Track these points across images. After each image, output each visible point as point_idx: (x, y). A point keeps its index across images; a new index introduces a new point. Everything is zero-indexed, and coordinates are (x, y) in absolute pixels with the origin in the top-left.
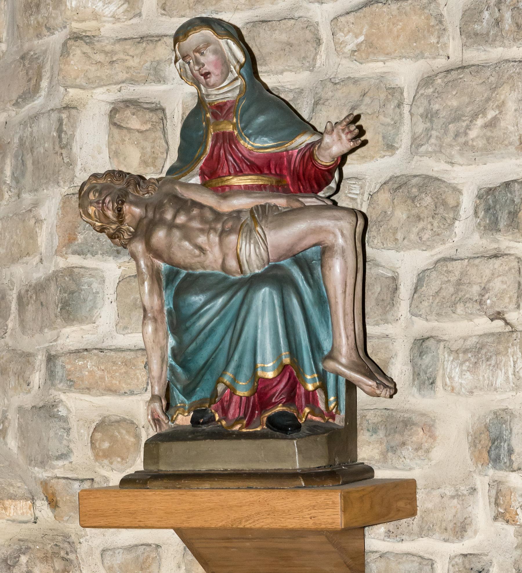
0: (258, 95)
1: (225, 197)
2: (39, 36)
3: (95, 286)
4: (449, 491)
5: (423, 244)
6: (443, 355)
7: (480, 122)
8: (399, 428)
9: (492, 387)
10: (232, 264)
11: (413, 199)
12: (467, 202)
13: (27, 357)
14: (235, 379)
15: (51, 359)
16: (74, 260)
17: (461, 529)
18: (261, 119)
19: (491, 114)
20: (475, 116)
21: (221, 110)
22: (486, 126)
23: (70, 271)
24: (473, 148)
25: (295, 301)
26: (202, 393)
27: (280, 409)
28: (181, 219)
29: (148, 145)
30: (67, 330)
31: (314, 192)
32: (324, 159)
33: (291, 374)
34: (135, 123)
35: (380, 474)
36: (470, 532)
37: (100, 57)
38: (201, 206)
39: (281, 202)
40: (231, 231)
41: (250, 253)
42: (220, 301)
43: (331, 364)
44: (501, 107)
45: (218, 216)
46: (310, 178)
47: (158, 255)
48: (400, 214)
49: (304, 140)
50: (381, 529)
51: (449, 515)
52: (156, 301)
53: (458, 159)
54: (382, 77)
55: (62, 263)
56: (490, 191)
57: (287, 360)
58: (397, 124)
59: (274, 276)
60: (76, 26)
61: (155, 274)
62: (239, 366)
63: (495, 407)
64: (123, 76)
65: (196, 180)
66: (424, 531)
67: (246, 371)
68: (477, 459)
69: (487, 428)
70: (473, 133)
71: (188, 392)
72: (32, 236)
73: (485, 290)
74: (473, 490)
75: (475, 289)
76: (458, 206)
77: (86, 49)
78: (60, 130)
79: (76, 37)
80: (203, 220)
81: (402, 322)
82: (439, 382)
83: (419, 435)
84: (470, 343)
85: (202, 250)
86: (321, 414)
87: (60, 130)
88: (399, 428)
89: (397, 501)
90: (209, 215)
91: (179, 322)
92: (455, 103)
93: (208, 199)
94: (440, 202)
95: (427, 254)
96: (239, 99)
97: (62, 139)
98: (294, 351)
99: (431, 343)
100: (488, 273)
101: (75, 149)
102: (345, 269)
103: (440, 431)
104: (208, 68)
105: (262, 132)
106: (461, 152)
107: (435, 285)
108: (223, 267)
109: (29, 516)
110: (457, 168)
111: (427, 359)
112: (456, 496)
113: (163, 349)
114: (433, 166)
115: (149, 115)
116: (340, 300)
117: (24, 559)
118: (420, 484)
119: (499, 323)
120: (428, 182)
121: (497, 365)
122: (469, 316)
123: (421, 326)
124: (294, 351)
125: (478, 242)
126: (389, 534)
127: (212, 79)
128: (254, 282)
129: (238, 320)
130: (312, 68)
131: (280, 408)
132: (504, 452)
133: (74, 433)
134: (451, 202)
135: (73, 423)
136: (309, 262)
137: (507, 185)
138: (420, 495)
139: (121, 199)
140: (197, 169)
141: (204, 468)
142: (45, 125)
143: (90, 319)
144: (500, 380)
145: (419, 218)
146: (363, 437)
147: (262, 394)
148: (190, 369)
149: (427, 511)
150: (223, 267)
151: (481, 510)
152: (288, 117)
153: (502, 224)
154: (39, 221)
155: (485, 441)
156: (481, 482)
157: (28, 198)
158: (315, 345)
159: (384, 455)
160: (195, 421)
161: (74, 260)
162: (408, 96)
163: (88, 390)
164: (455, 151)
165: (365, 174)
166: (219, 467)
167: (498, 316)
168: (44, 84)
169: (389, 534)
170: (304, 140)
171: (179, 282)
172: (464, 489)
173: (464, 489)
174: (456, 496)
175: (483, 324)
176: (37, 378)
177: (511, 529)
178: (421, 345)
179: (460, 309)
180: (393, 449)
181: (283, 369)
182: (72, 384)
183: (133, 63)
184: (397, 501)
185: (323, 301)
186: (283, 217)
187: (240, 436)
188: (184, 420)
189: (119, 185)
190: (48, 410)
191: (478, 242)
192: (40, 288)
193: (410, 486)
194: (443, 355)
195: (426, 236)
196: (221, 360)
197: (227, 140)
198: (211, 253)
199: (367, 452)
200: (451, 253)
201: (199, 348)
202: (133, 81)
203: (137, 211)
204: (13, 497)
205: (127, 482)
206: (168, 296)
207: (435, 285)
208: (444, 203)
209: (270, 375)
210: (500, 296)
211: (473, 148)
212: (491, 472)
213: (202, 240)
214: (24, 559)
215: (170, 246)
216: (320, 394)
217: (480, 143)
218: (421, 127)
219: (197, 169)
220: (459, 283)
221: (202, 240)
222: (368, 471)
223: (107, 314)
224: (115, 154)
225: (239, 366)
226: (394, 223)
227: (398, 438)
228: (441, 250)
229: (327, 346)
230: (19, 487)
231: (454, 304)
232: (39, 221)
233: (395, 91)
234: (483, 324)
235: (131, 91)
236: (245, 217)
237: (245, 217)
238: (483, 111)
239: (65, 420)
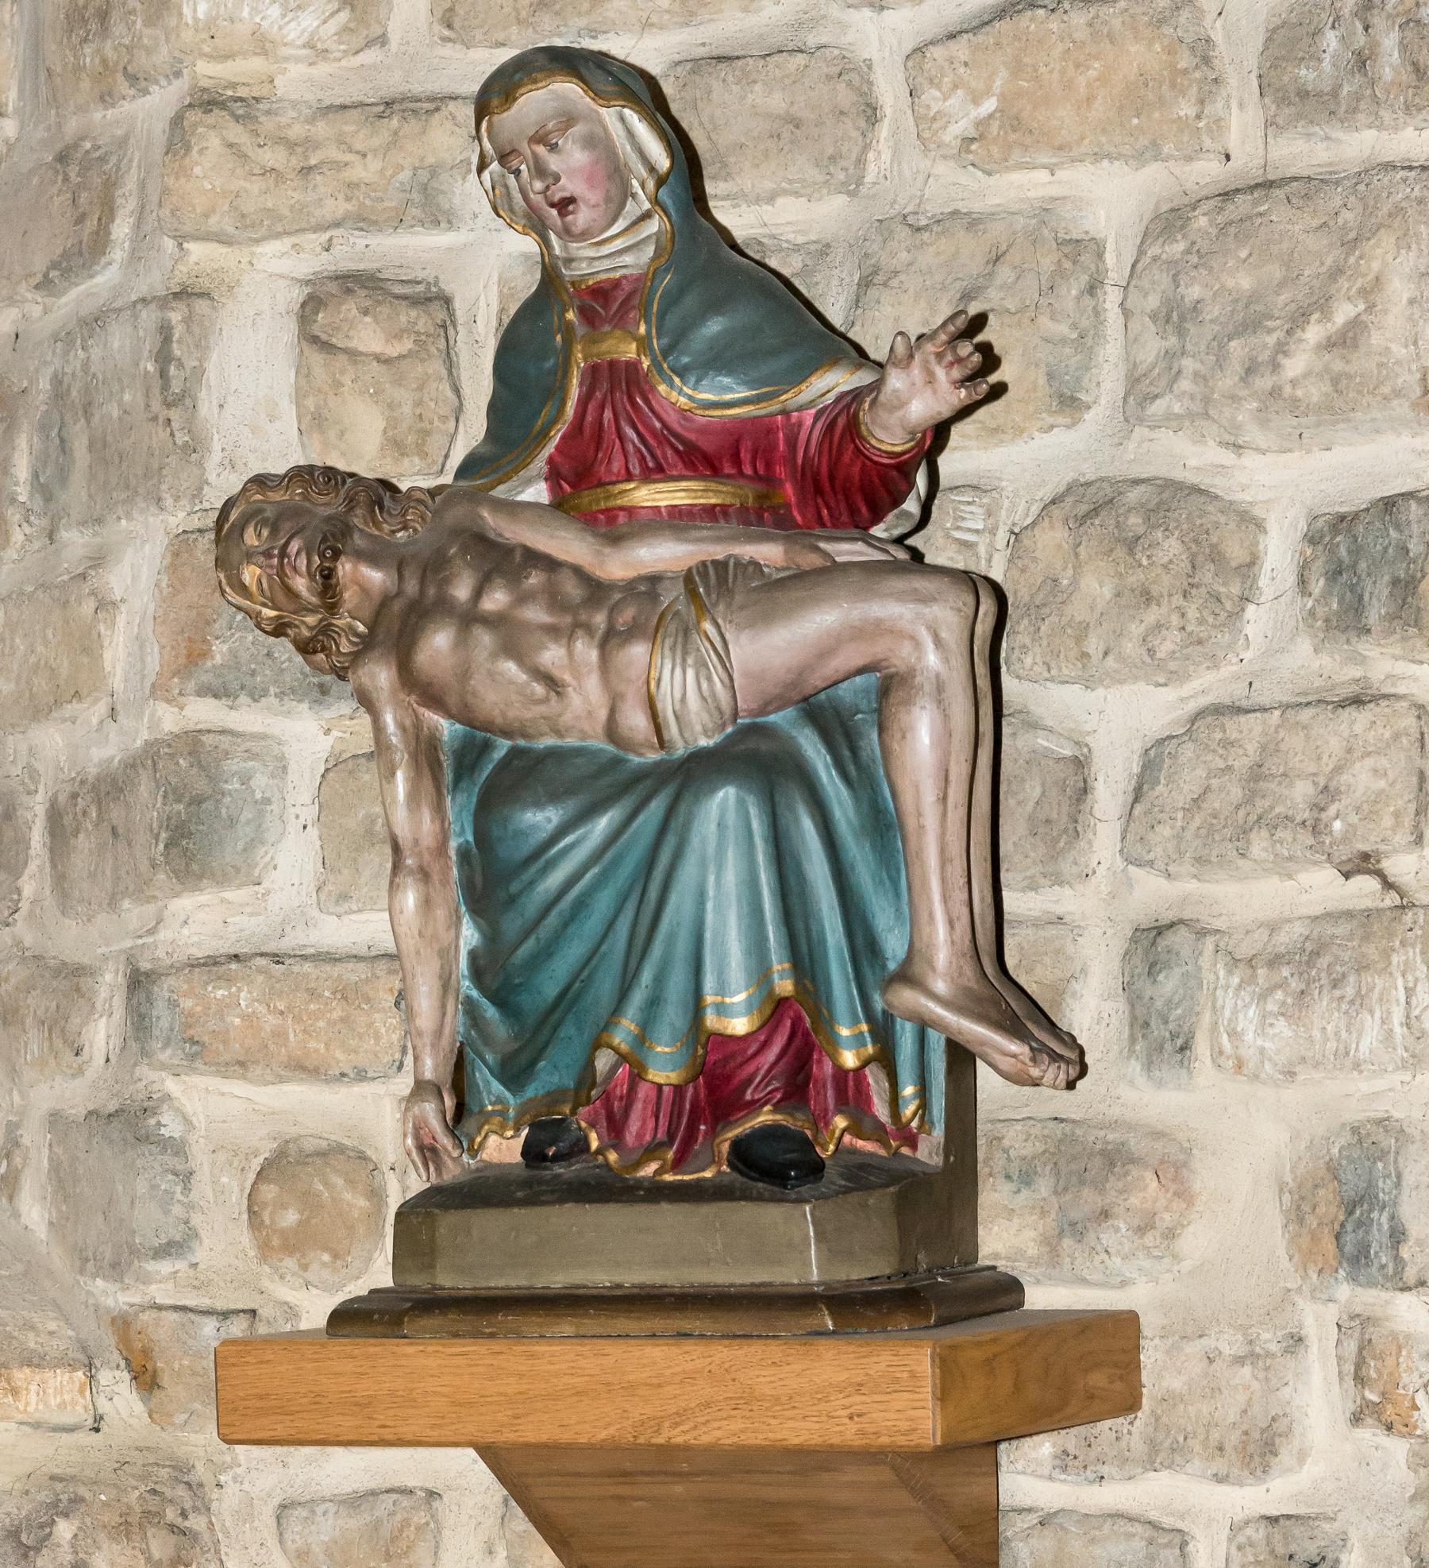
0: (707, 261)
1: (615, 539)
2: (107, 98)
3: (261, 782)
4: (1229, 1344)
5: (1158, 669)
6: (1214, 971)
7: (1313, 333)
8: (1093, 1170)
9: (1347, 1060)
10: (636, 721)
11: (1132, 545)
12: (1279, 553)
13: (74, 978)
14: (642, 1038)
15: (139, 982)
16: (204, 712)
17: (1261, 1447)
18: (714, 326)
19: (1344, 312)
20: (1299, 318)
21: (604, 302)
22: (1330, 345)
23: (192, 742)
24: (1295, 406)
25: (808, 824)
26: (552, 1075)
27: (766, 1120)
28: (496, 600)
29: (405, 398)
30: (185, 903)
31: (859, 524)
32: (888, 435)
33: (796, 1023)
34: (369, 337)
35: (1039, 1297)
36: (1285, 1456)
37: (273, 157)
38: (551, 564)
39: (769, 553)
40: (632, 633)
41: (685, 693)
42: (603, 824)
43: (907, 997)
44: (1371, 292)
45: (596, 590)
46: (849, 488)
47: (433, 698)
48: (1096, 586)
49: (833, 382)
50: (1044, 1447)
51: (1229, 1408)
52: (428, 823)
53: (1253, 434)
54: (1045, 211)
55: (169, 720)
56: (1342, 522)
57: (785, 986)
58: (1086, 340)
59: (750, 756)
60: (208, 71)
61: (425, 751)
62: (654, 1002)
63: (1355, 1113)
64: (337, 207)
65: (537, 492)
66: (1162, 1454)
67: (673, 1016)
68: (1305, 1255)
69: (1334, 1171)
70: (1295, 365)
71: (514, 1073)
72: (88, 646)
73: (1328, 793)
74: (1296, 1341)
75: (1302, 792)
76: (1253, 563)
77: (237, 133)
78: (164, 357)
79: (209, 101)
80: (556, 601)
81: (1101, 881)
82: (1202, 1046)
83: (1148, 1191)
84: (1287, 938)
85: (552, 683)
86: (878, 1133)
87: (164, 357)
88: (1093, 1170)
89: (1088, 1372)
90: (572, 589)
91: (489, 880)
92: (1245, 282)
93: (569, 545)
94: (1205, 553)
95: (1169, 694)
96: (655, 272)
97: (171, 380)
98: (805, 959)
99: (1179, 939)
100: (1335, 746)
101: (206, 407)
102: (944, 736)
103: (1204, 1179)
104: (568, 186)
105: (718, 360)
106: (1262, 416)
107: (1190, 781)
108: (612, 731)
109: (80, 1413)
110: (1250, 460)
111: (1168, 983)
112: (1250, 1357)
113: (446, 955)
114: (1186, 455)
115: (407, 315)
116: (931, 821)
117: (64, 1530)
118: (1149, 1324)
119: (1367, 884)
120: (1172, 498)
121: (1360, 1000)
122: (1284, 866)
123: (1152, 893)
124: (805, 959)
125: (1309, 662)
126: (1064, 1461)
127: (582, 218)
128: (694, 772)
129: (652, 877)
130: (853, 187)
131: (765, 1117)
132: (1378, 1236)
133: (202, 1185)
134: (1236, 553)
135: (200, 1158)
136: (847, 717)
137: (1389, 505)
138: (1150, 1356)
139: (332, 544)
140: (540, 464)
141: (557, 1280)
142: (122, 343)
143: (245, 874)
144: (1369, 1039)
145: (1147, 597)
146: (993, 1195)
147: (718, 1078)
148: (519, 1010)
149: (1169, 1399)
150: (612, 731)
151: (1317, 1397)
152: (787, 321)
153: (1374, 614)
154: (106, 605)
155: (1328, 1206)
156: (1317, 1320)
157: (75, 541)
158: (864, 945)
159: (1051, 1245)
160: (533, 1153)
161: (204, 712)
162: (1116, 264)
163: (241, 1066)
164: (1245, 413)
165: (1001, 476)
166: (600, 1278)
167: (1365, 864)
168: (121, 229)
169: (1064, 1461)
170: (833, 382)
171: (490, 773)
172: (1269, 1339)
173: (1269, 1339)
174: (1250, 1357)
175: (1322, 888)
176: (102, 1034)
177: (1398, 1448)
178: (1152, 943)
179: (1259, 844)
180: (1076, 1229)
181: (776, 1010)
182: (197, 1051)
183: (365, 171)
184: (1088, 1372)
185: (884, 825)
186: (775, 593)
187: (657, 1192)
188: (503, 1149)
189: (327, 505)
190: (130, 1123)
191: (1309, 662)
192: (109, 788)
193: (1121, 1330)
194: (1214, 971)
195: (1166, 645)
196: (606, 985)
197: (620, 383)
198: (578, 693)
199: (1004, 1236)
200: (1236, 692)
201: (546, 953)
202: (363, 222)
203: (375, 576)
204: (35, 1361)
205: (349, 1318)
206: (459, 810)
207: (1190, 781)
208: (1216, 556)
209: (740, 1026)
210: (1369, 811)
211: (1295, 406)
212: (1344, 1291)
213: (552, 656)
214: (64, 1530)
215: (464, 674)
216: (875, 1079)
217: (1315, 392)
218: (1151, 347)
219: (540, 464)
220: (1257, 774)
221: (552, 656)
222: (1008, 1290)
223: (292, 859)
224: (315, 422)
225: (654, 1002)
226: (1078, 610)
227: (1090, 1199)
228: (1208, 684)
229: (894, 947)
230: (51, 1333)
231: (1243, 833)
232: (106, 605)
233: (1080, 250)
234: (1322, 888)
235: (358, 250)
236: (672, 595)
237: (672, 595)
238: (1322, 305)
239: (178, 1148)
